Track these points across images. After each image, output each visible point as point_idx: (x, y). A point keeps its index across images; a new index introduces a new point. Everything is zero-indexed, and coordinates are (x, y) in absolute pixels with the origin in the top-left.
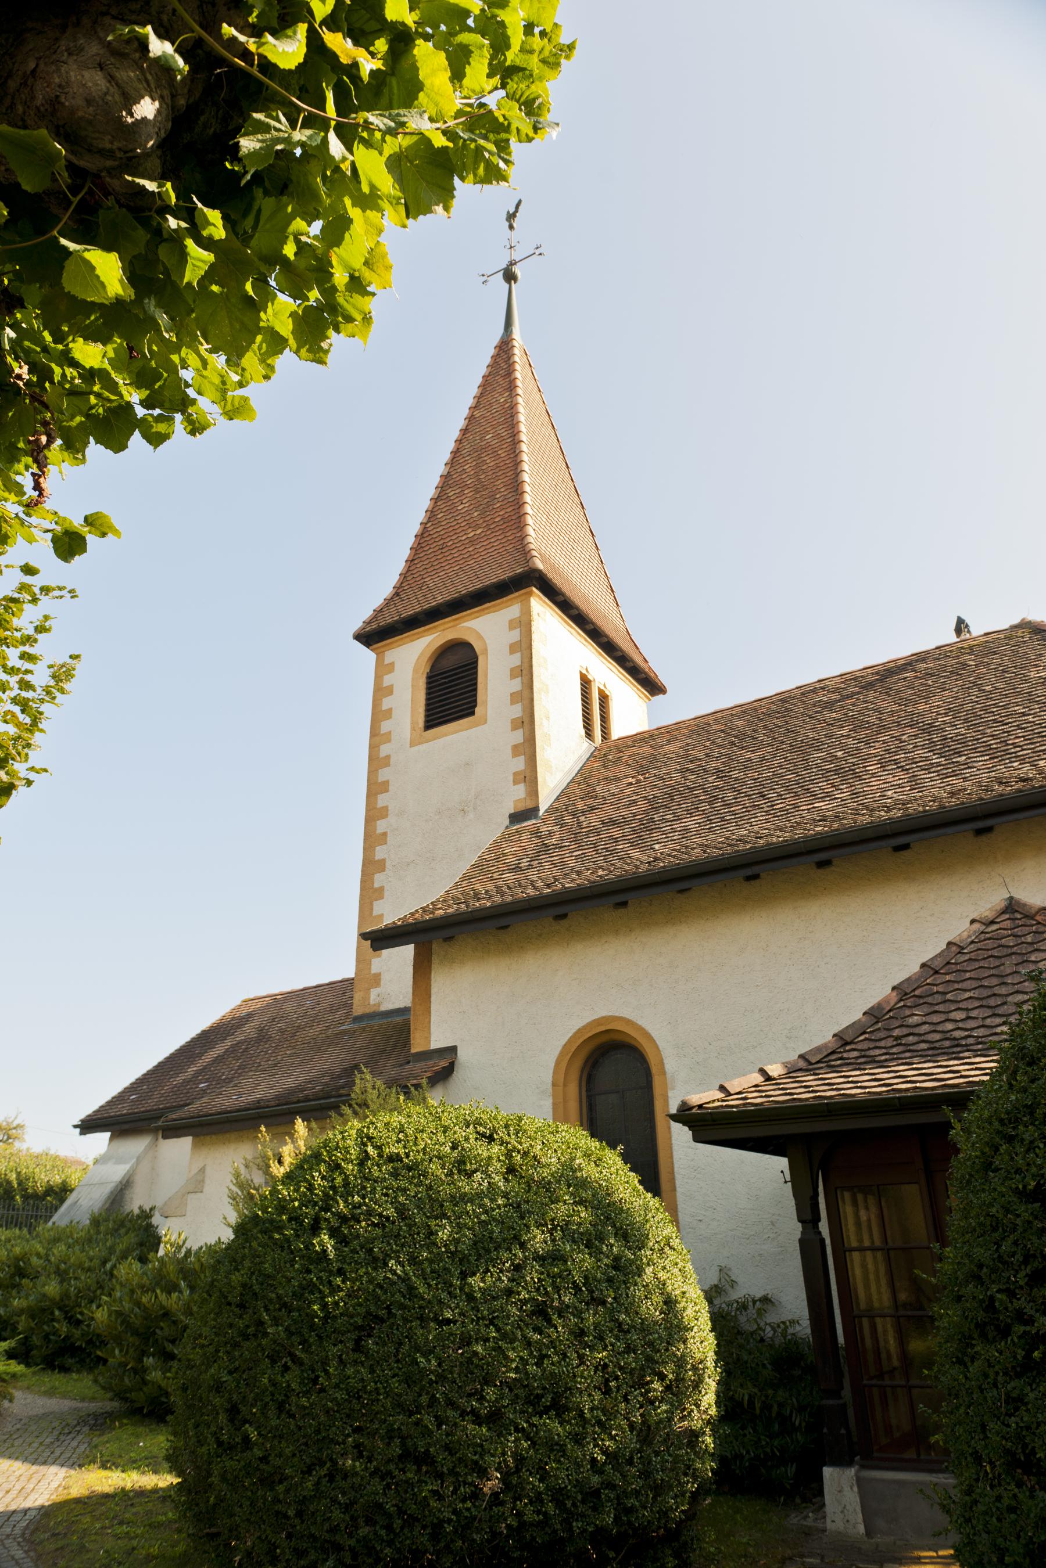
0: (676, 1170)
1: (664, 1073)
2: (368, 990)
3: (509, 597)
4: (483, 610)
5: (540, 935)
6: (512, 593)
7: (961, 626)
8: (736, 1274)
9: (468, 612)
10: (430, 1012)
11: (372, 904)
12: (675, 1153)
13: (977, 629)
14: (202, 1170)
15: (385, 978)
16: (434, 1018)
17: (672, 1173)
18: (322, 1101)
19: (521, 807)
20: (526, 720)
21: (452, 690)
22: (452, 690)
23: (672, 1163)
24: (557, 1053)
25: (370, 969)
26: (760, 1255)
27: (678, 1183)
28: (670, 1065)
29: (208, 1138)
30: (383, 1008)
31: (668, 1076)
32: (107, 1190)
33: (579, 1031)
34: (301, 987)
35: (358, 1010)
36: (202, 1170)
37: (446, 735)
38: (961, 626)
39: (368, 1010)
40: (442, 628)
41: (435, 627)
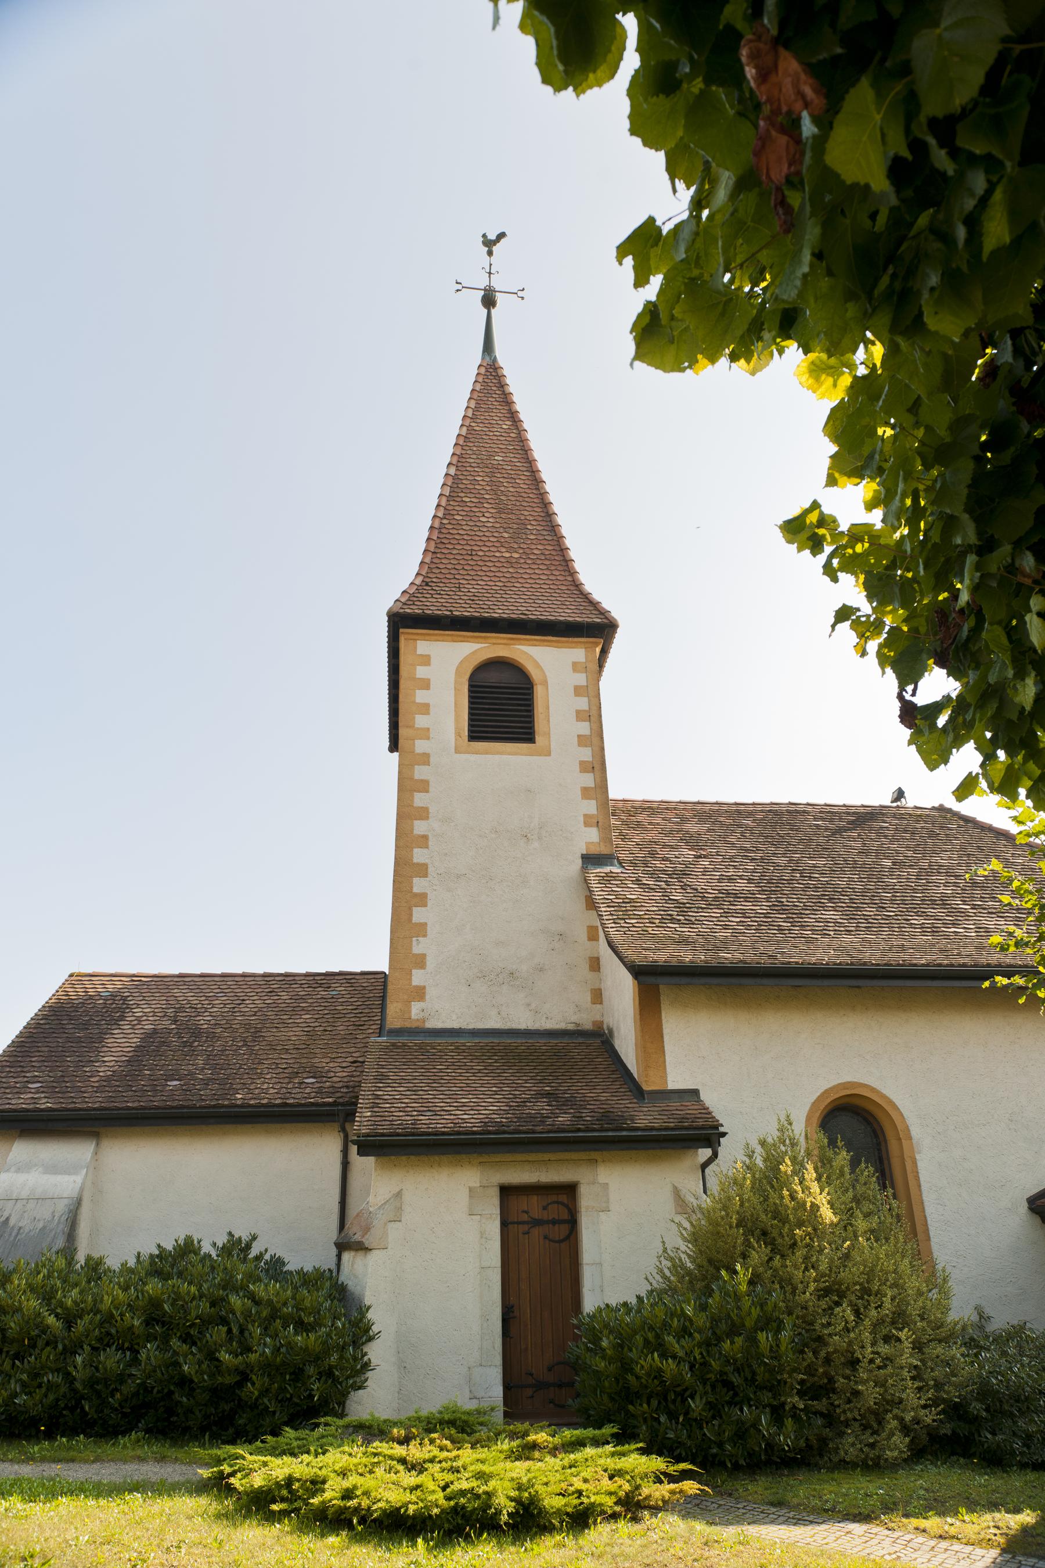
0: (929, 1222)
1: (910, 1138)
2: (408, 1003)
3: (576, 639)
4: (544, 641)
5: (778, 997)
6: (582, 636)
7: (900, 794)
8: (988, 1311)
9: (528, 637)
10: (664, 1052)
11: (410, 909)
12: (926, 1208)
13: (911, 801)
14: (399, 1195)
15: (431, 993)
16: (669, 1058)
17: (926, 1225)
18: (610, 1134)
19: (595, 850)
20: (597, 767)
21: (502, 709)
22: (502, 709)
23: (925, 1217)
24: (807, 1108)
25: (410, 979)
26: (1006, 1296)
27: (932, 1234)
28: (915, 1132)
29: (404, 1158)
30: (430, 1025)
31: (914, 1141)
32: (61, 1207)
33: (827, 1092)
34: (176, 971)
35: (393, 1021)
36: (399, 1195)
37: (501, 753)
38: (900, 794)
39: (408, 1025)
40: (494, 641)
41: (485, 638)
